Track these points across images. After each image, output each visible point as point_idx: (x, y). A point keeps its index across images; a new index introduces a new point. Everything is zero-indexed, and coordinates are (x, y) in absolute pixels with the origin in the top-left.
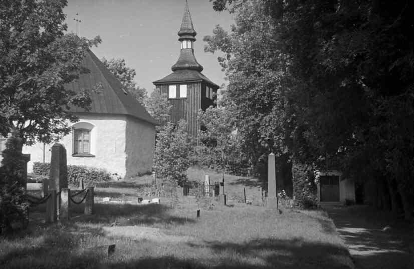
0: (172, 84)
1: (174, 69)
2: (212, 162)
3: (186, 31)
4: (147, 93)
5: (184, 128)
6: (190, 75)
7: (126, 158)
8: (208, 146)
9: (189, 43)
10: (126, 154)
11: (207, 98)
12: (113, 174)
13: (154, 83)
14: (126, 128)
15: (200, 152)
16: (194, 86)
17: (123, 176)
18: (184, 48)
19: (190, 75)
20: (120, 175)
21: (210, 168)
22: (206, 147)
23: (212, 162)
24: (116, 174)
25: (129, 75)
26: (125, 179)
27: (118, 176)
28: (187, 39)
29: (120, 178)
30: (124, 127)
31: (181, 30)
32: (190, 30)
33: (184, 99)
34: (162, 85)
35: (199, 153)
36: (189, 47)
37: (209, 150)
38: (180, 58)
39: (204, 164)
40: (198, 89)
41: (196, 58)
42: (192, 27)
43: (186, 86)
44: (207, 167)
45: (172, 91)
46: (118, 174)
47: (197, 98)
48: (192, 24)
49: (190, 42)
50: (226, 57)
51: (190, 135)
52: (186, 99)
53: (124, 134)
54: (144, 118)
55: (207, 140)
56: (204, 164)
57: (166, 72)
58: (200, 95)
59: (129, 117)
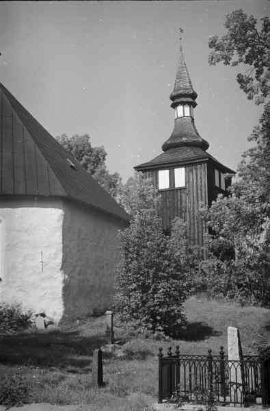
0: (163, 168)
1: (166, 148)
2: (229, 287)
3: (181, 92)
4: (121, 179)
5: (181, 232)
6: (189, 153)
7: (64, 281)
8: (222, 260)
9: (187, 109)
10: (65, 273)
11: (217, 187)
12: (37, 315)
13: (135, 168)
14: (64, 222)
15: (210, 271)
16: (196, 169)
17: (57, 318)
18: (232, 381)
19: (189, 153)
20: (51, 316)
21: (227, 297)
22: (219, 261)
23: (229, 287)
24: (43, 315)
25: (98, 157)
26: (61, 323)
27: (46, 319)
28: (183, 103)
29: (51, 323)
30: (58, 221)
31: (174, 91)
32: (187, 89)
33: (180, 189)
34: (149, 169)
35: (207, 271)
36: (187, 114)
37: (224, 266)
38: (175, 130)
39: (216, 291)
40: (202, 172)
41: (197, 128)
42: (191, 86)
43: (183, 169)
44: (221, 294)
45: (163, 177)
46: (47, 314)
47: (201, 186)
48: (190, 82)
49: (189, 108)
50: (254, 75)
51: (192, 242)
52: (185, 188)
53: (59, 234)
54: (91, 201)
55: (220, 249)
56: (216, 291)
57: (154, 152)
58: (205, 181)
59: (68, 202)
